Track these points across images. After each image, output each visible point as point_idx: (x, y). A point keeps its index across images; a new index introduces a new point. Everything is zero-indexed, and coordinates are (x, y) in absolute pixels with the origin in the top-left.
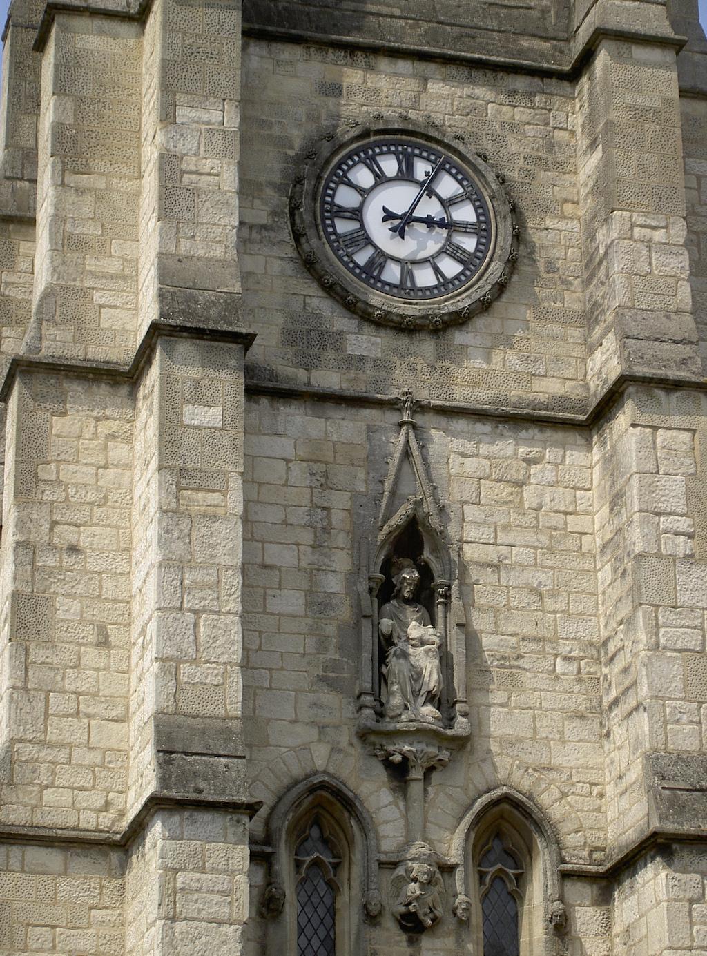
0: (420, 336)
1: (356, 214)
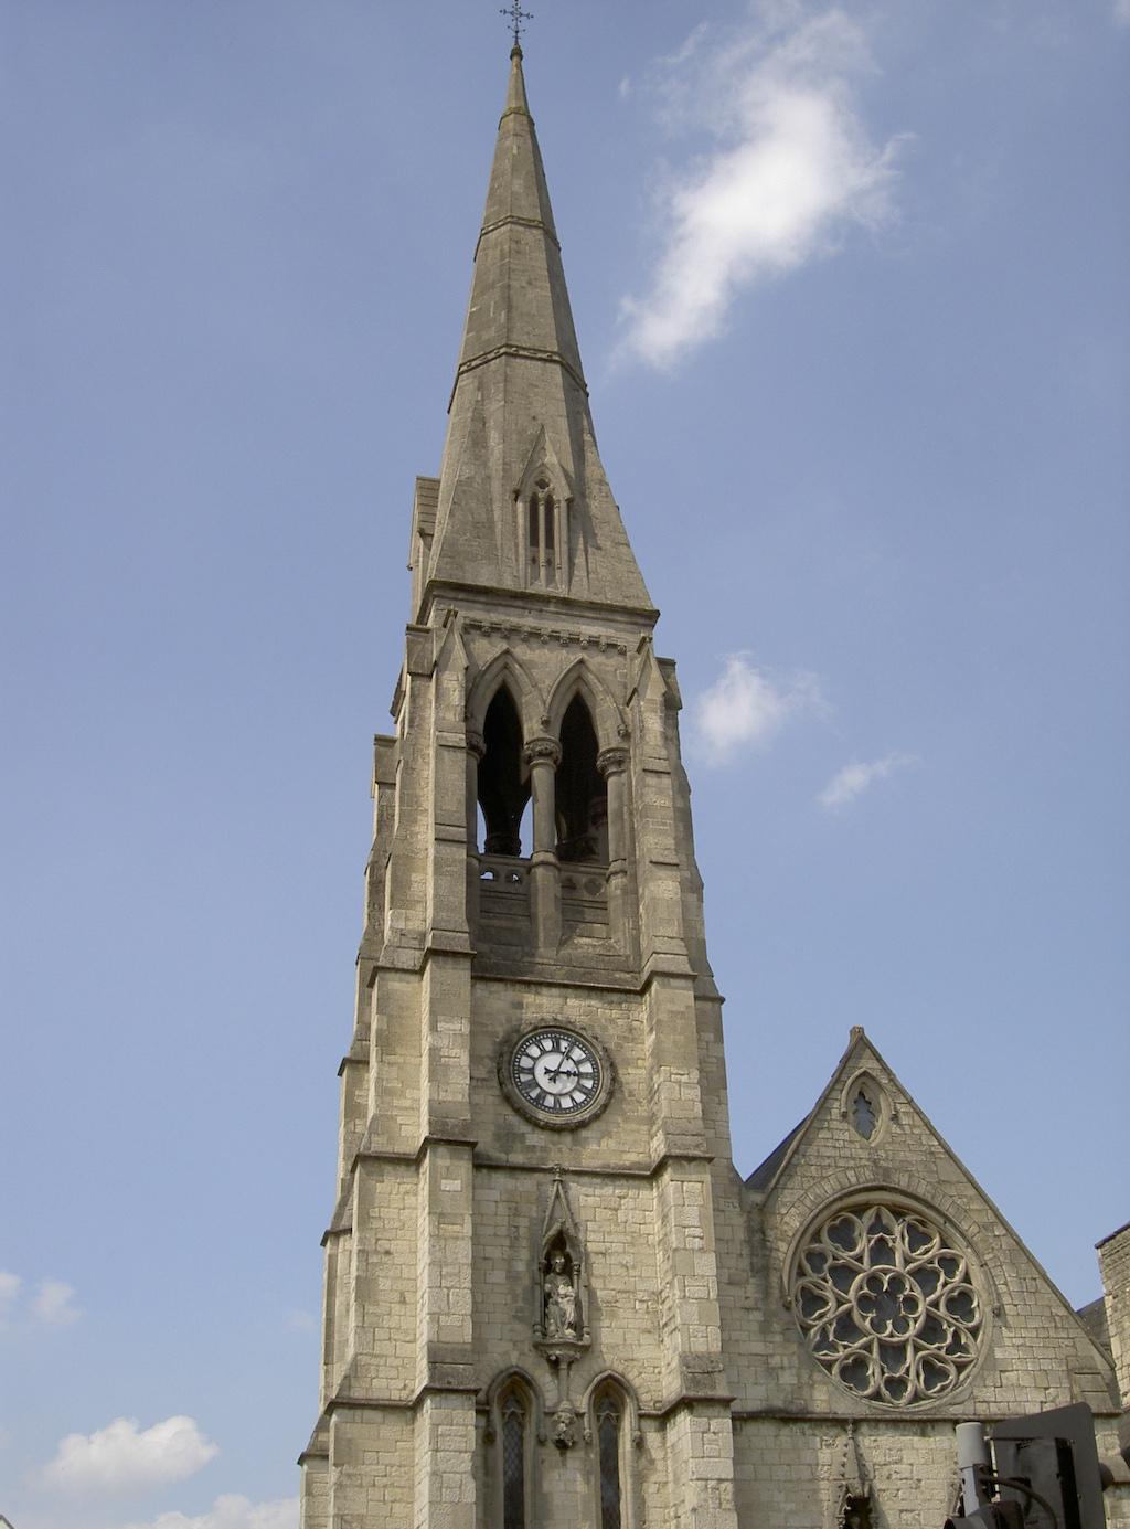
0: (563, 1133)
1: (531, 1071)
